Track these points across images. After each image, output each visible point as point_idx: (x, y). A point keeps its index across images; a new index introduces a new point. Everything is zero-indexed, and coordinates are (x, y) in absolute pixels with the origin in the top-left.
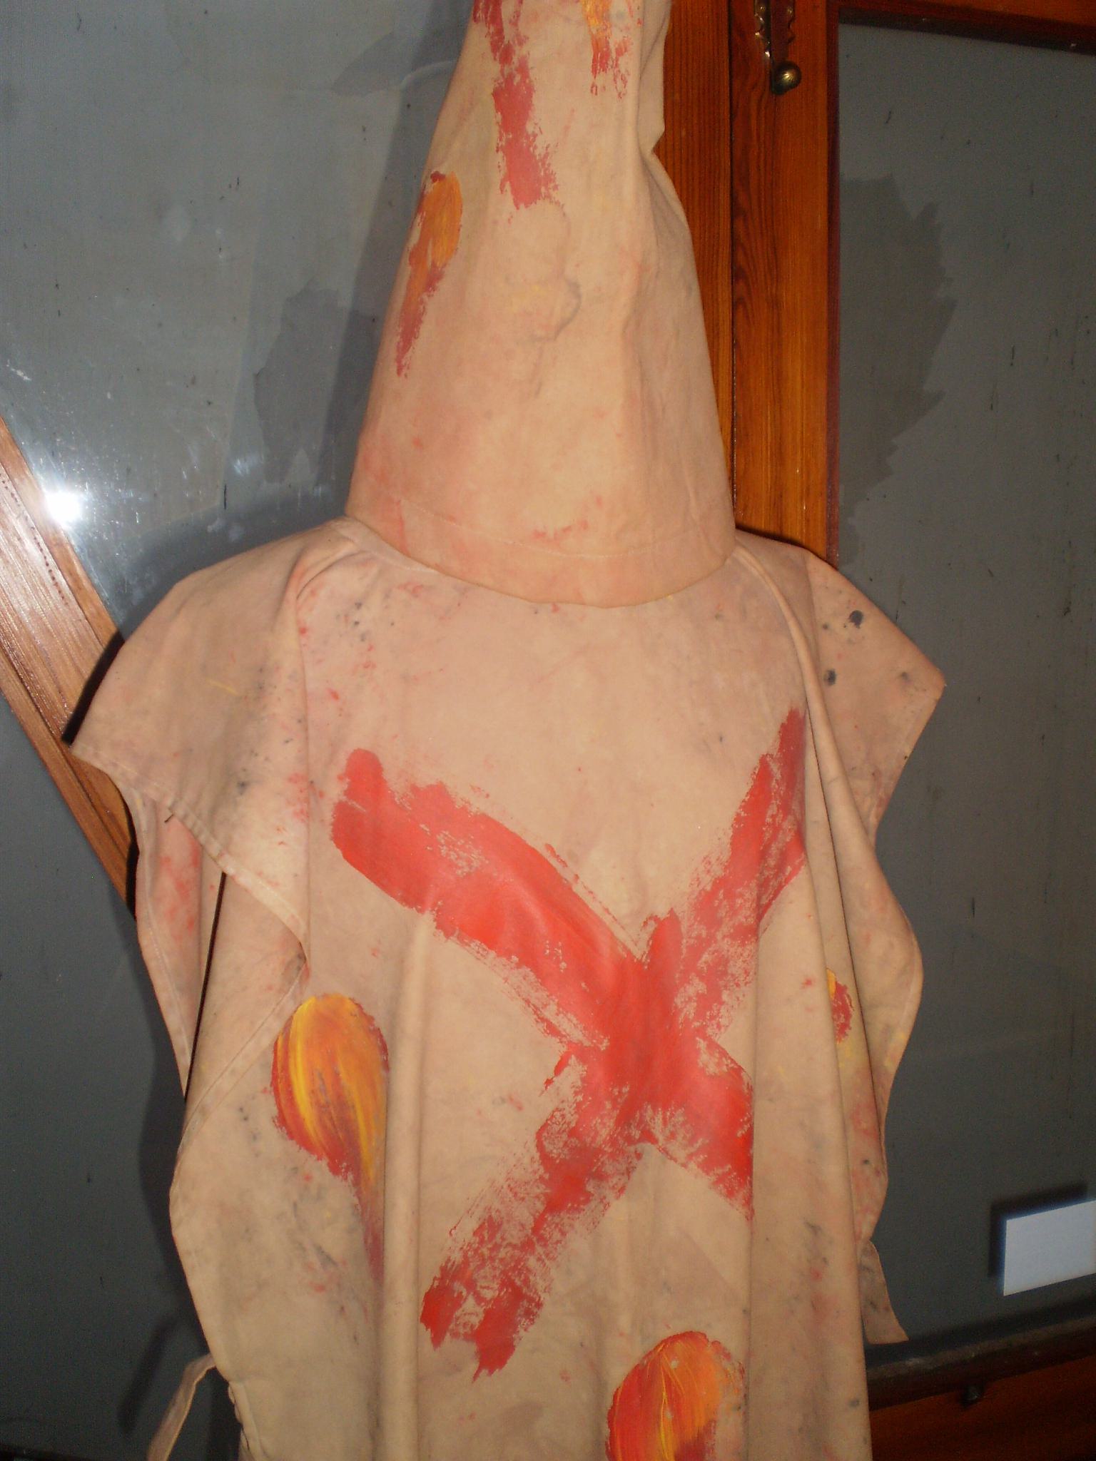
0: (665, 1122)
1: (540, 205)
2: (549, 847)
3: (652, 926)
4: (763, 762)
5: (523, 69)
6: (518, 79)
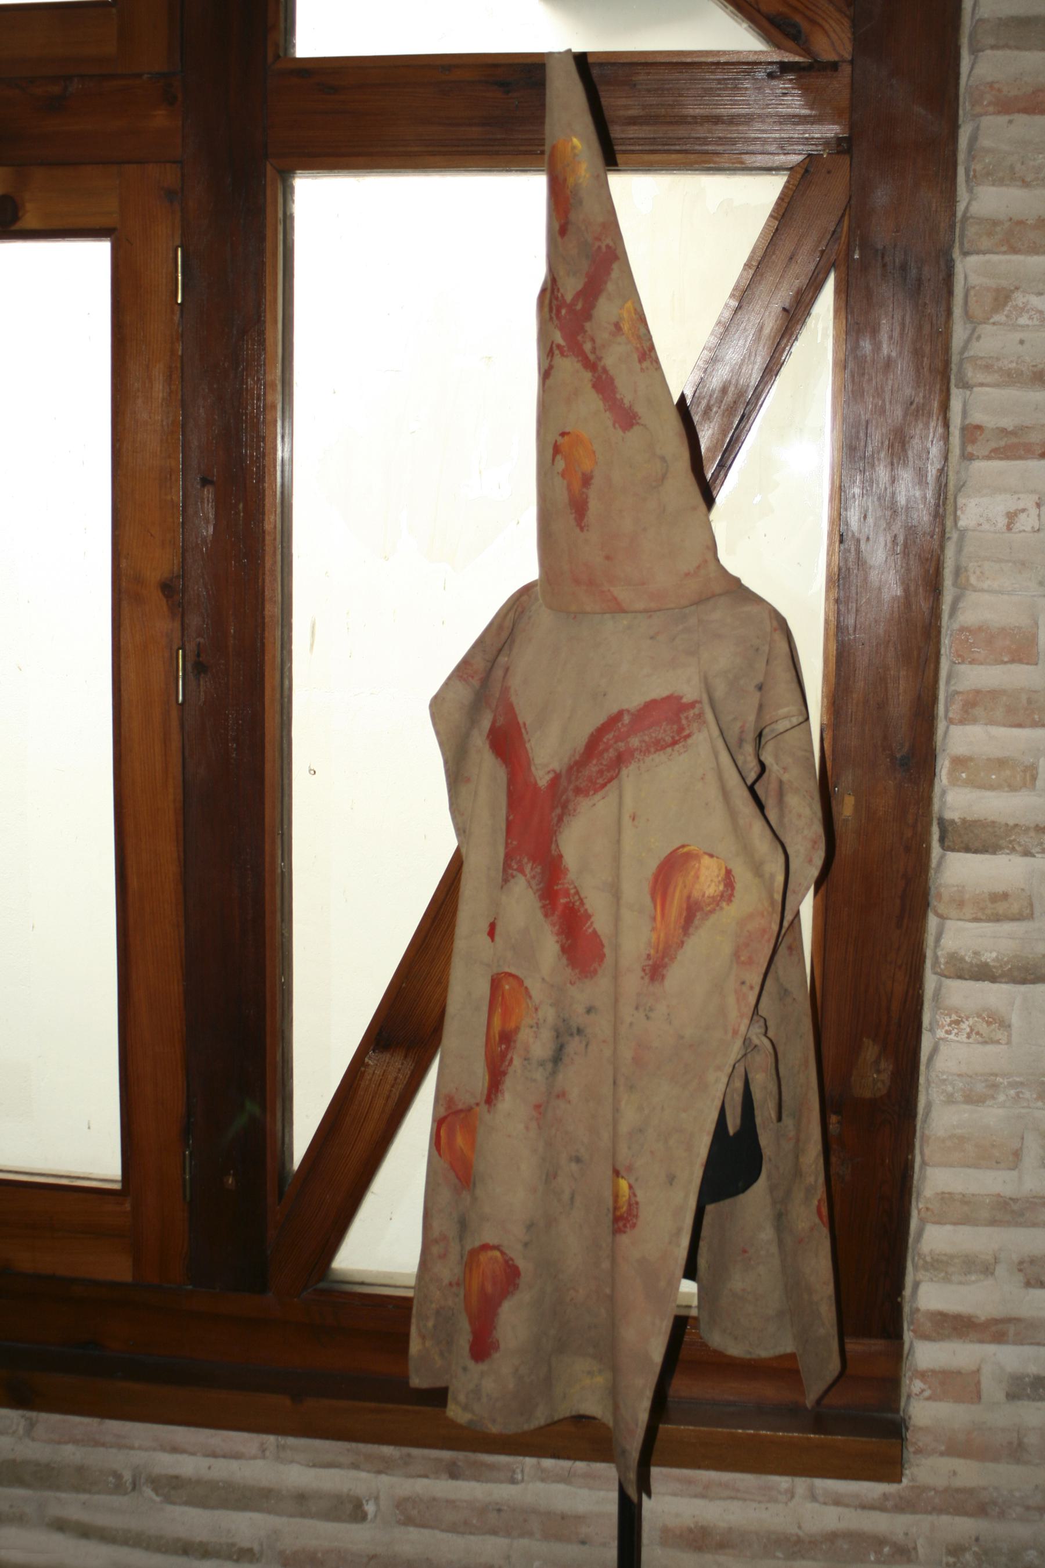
0: (532, 869)
1: (636, 428)
2: (525, 724)
3: (551, 775)
4: (620, 714)
5: (605, 370)
6: (604, 376)
